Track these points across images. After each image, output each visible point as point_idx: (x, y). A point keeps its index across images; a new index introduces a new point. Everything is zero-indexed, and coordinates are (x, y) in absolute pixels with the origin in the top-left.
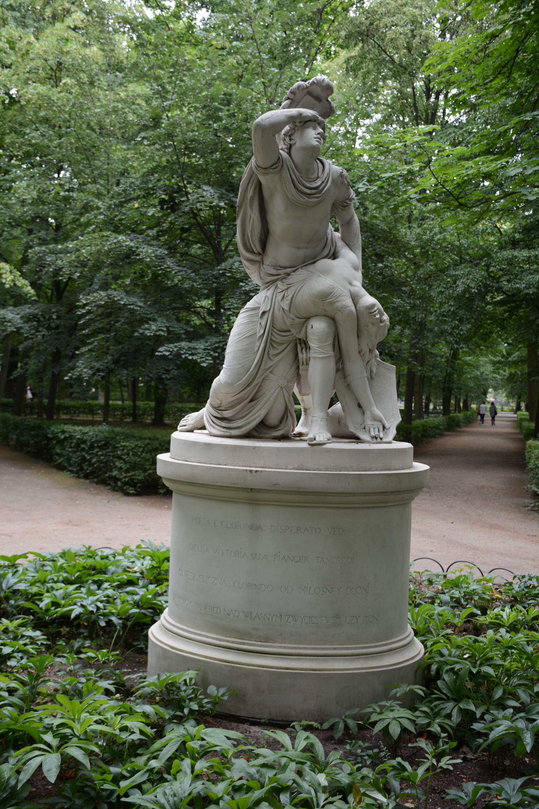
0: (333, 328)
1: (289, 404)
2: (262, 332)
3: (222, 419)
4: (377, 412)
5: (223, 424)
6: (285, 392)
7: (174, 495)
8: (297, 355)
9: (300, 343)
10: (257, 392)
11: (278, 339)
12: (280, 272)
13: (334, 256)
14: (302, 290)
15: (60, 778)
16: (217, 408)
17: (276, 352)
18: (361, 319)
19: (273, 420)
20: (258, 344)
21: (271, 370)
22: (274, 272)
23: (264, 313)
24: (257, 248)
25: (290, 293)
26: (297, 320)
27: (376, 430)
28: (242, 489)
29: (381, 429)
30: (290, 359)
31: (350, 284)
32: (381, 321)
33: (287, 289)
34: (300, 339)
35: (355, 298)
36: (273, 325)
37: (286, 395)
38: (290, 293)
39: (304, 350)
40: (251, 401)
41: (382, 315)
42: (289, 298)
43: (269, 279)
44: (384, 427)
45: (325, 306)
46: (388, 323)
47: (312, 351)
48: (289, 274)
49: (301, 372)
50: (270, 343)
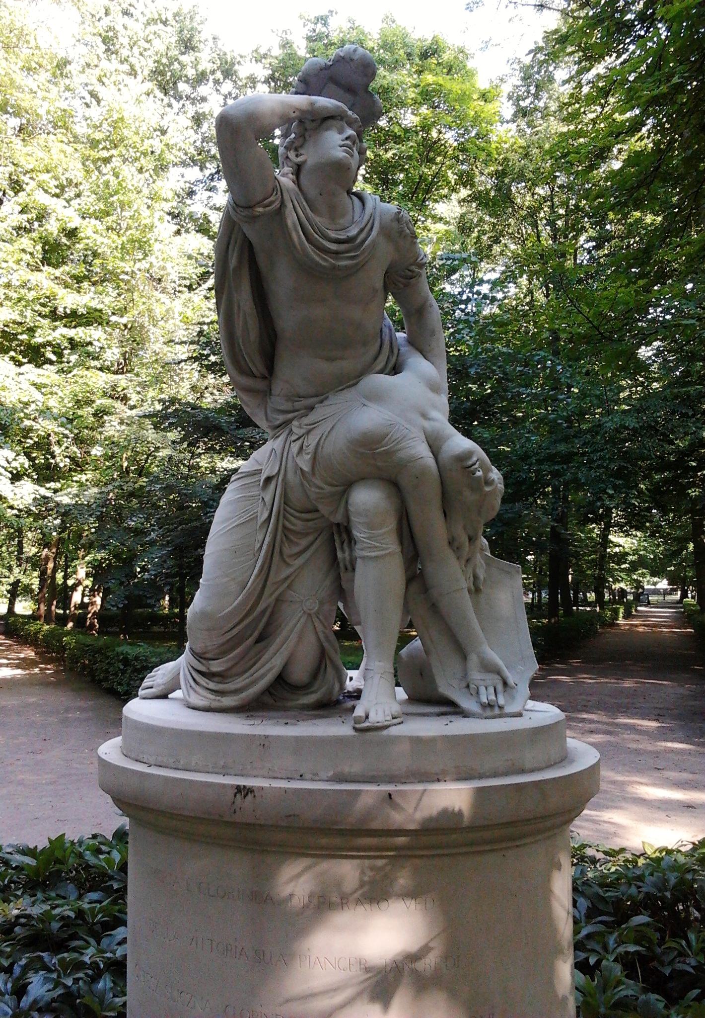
1: (325, 644)
2: (266, 515)
4: (494, 657)
5: (212, 685)
6: (317, 624)
10: (268, 624)
11: (299, 525)
12: (297, 405)
13: (396, 370)
14: (334, 433)
16: (198, 656)
17: (296, 550)
18: (453, 478)
19: (300, 673)
20: (260, 538)
21: (290, 582)
22: (287, 406)
23: (268, 480)
24: (258, 367)
25: (312, 441)
26: (328, 489)
27: (491, 690)
29: (500, 687)
31: (424, 416)
32: (488, 482)
33: (308, 432)
34: (338, 525)
35: (434, 444)
36: (286, 500)
38: (312, 441)
39: (345, 545)
40: (258, 641)
41: (487, 471)
42: (311, 449)
43: (281, 418)
44: (505, 684)
45: (377, 460)
46: (501, 486)
47: (358, 546)
48: (311, 408)
49: (345, 585)
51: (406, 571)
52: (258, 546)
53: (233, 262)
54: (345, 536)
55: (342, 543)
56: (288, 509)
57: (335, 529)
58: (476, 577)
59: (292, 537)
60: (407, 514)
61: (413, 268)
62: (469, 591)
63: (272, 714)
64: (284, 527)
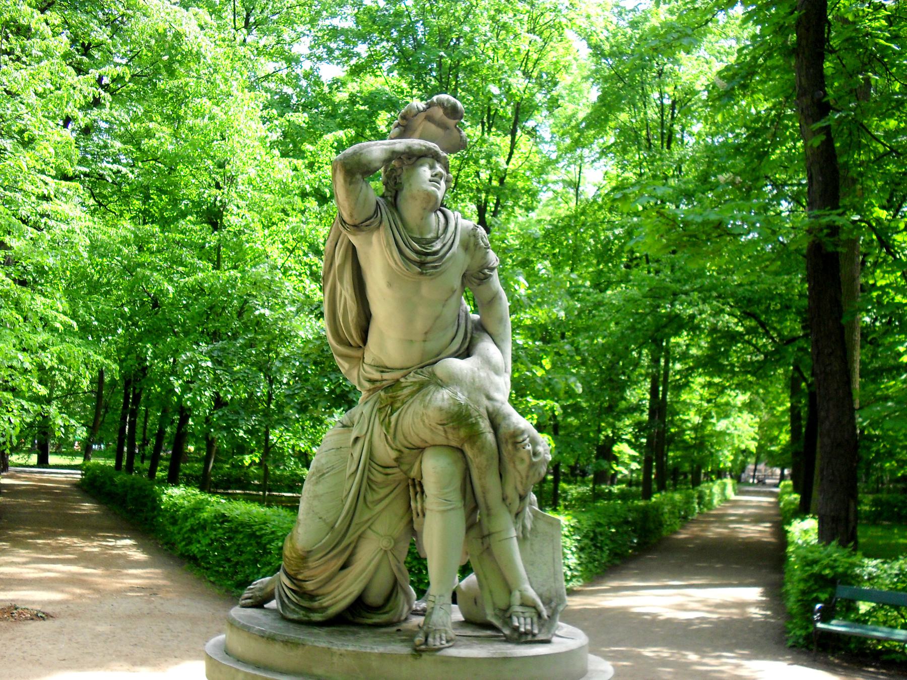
0: (461, 465)
2: (354, 468)
3: (284, 618)
8: (410, 506)
9: (414, 486)
15: (566, 317)
19: (375, 596)
20: (347, 487)
24: (356, 339)
27: (529, 621)
29: (535, 619)
30: (399, 507)
34: (413, 480)
36: (371, 456)
37: (393, 562)
39: (418, 496)
49: (415, 527)
50: (367, 484)
51: (467, 520)
52: (345, 494)
53: (338, 261)
54: (418, 489)
55: (416, 494)
56: (373, 464)
57: (410, 482)
58: (524, 527)
59: (374, 486)
60: (355, 547)
61: (486, 271)
62: (518, 537)
64: (368, 478)
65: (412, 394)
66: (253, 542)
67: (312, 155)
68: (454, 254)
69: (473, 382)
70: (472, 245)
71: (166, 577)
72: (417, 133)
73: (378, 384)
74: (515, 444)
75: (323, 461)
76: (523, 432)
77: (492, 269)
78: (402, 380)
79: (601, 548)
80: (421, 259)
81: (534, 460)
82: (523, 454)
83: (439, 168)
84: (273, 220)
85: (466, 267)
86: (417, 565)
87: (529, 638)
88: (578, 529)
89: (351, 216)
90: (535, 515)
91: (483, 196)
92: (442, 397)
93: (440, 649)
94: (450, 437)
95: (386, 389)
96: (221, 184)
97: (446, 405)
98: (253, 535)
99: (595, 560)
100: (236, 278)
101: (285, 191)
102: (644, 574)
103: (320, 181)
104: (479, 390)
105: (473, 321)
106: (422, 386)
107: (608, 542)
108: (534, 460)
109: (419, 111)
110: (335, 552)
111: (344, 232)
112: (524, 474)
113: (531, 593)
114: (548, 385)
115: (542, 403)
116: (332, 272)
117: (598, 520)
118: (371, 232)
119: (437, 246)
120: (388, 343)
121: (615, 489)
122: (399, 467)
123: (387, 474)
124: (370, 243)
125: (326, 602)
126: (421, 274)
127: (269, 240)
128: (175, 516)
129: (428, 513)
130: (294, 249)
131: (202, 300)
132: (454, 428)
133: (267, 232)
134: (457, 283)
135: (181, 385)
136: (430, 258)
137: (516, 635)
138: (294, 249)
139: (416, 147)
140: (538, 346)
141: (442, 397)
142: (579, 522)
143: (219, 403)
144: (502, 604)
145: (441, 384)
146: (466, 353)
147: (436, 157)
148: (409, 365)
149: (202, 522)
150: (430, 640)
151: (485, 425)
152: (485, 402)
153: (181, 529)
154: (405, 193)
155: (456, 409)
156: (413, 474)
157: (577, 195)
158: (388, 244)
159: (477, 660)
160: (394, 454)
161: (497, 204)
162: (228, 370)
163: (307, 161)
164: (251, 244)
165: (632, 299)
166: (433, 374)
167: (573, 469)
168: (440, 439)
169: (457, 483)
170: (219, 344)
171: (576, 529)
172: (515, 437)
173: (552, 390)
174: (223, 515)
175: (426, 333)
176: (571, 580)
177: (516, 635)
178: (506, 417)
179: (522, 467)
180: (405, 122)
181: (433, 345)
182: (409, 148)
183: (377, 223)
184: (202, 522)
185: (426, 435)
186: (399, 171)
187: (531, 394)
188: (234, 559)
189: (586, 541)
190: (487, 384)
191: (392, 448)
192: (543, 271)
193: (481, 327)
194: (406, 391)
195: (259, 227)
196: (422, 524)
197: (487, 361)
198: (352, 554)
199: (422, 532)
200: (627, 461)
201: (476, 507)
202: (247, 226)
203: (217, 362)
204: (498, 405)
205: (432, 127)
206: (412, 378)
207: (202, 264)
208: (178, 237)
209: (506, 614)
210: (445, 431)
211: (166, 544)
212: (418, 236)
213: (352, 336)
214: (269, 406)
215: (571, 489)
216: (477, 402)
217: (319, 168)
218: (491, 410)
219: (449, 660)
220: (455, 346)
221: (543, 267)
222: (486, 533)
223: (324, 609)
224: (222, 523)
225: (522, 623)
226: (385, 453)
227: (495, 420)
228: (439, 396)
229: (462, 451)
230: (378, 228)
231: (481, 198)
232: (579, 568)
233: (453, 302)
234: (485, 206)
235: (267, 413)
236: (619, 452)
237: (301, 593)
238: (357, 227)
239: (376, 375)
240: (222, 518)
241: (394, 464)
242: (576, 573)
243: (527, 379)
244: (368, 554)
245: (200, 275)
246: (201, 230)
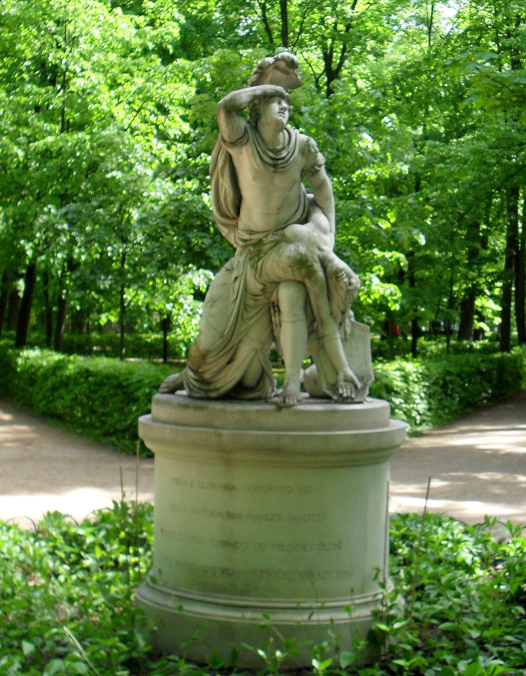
2: (235, 296)
7: (157, 458)
8: (271, 321)
9: (274, 307)
19: (251, 380)
24: (232, 212)
27: (349, 390)
28: (347, 453)
29: (353, 389)
30: (264, 321)
34: (273, 303)
37: (261, 357)
50: (244, 307)
53: (220, 164)
54: (276, 309)
55: (275, 312)
57: (271, 305)
58: (345, 332)
60: (237, 348)
61: (316, 167)
62: (342, 339)
63: (485, 414)
65: (271, 248)
66: (120, 392)
67: (153, 12)
68: (295, 159)
69: (310, 239)
70: (306, 152)
71: (35, 431)
72: (269, 78)
73: (248, 243)
74: (337, 278)
75: (215, 293)
76: (341, 270)
77: (320, 166)
78: (264, 239)
79: (451, 396)
80: (274, 163)
81: (350, 288)
82: (342, 284)
83: (284, 104)
84: (119, 81)
85: (302, 166)
86: (276, 357)
87: (350, 400)
88: (427, 376)
89: (230, 137)
90: (353, 324)
91: (329, 42)
92: (290, 250)
93: (293, 406)
94: (296, 274)
95: (254, 245)
96: (63, 44)
97: (293, 254)
98: (120, 386)
99: (444, 407)
100: (85, 141)
101: (127, 50)
102: (495, 420)
103: (162, 37)
104: (312, 244)
105: (309, 200)
106: (277, 243)
107: (459, 390)
108: (350, 288)
109: (270, 65)
110: (220, 354)
111: (224, 146)
112: (343, 297)
113: (351, 373)
114: (392, 237)
115: (388, 255)
116: (216, 171)
117: (448, 369)
118: (242, 146)
119: (284, 154)
120: (255, 214)
121: (477, 345)
122: (263, 294)
123: (256, 300)
124: (241, 153)
125: (218, 385)
126: (274, 172)
127: (115, 101)
128: (33, 376)
129: (283, 324)
130: (140, 110)
131: (51, 163)
132: (298, 269)
133: (112, 93)
134: (297, 176)
135: (31, 248)
136: (280, 162)
137: (341, 399)
138: (140, 110)
139: (269, 91)
140: (382, 201)
141: (290, 250)
142: (428, 369)
143: (72, 264)
144: (332, 380)
145: (289, 241)
146: (305, 220)
147: (281, 96)
148: (267, 229)
149: (64, 379)
150: (287, 400)
151: (317, 266)
152: (318, 252)
153: (41, 388)
154: (263, 120)
155: (299, 257)
156: (273, 299)
157: (429, 33)
158: (253, 154)
159: (316, 412)
160: (260, 287)
161: (344, 50)
162: (82, 230)
163: (148, 19)
164: (97, 105)
165: (479, 151)
166: (284, 235)
167: (435, 324)
168: (289, 276)
169: (301, 303)
170: (72, 206)
171: (425, 377)
172: (337, 273)
173: (396, 241)
174: (87, 371)
175: (278, 209)
176: (420, 424)
177: (341, 399)
178: (331, 261)
179: (342, 293)
180: (260, 71)
181: (284, 216)
182: (265, 92)
183: (245, 141)
184: (64, 379)
185: (281, 274)
186: (258, 106)
187: (377, 247)
188: (101, 410)
189: (436, 388)
190: (318, 240)
191: (259, 283)
192: (390, 124)
193: (314, 203)
194: (267, 247)
195: (104, 88)
196: (279, 332)
197: (319, 226)
198: (235, 354)
199: (279, 337)
200: (490, 316)
201: (314, 320)
202: (93, 87)
203: (71, 223)
204: (326, 253)
205: (279, 74)
206: (271, 238)
207: (47, 126)
208: (23, 99)
209: (334, 387)
210: (293, 271)
211: (25, 405)
212: (271, 147)
213: (229, 211)
214: (123, 265)
215: (431, 345)
216: (313, 252)
217: (161, 24)
218: (321, 256)
219: (298, 413)
220: (298, 216)
221: (390, 121)
222: (320, 335)
223: (218, 389)
224: (87, 378)
225: (345, 391)
226: (255, 286)
227: (324, 262)
228: (288, 249)
229: (302, 283)
230: (246, 143)
231: (326, 44)
232: (428, 413)
233: (295, 188)
234: (332, 52)
235: (121, 273)
236: (482, 307)
237: (202, 381)
238: (233, 144)
239: (247, 237)
240: (87, 373)
241: (259, 293)
242: (425, 418)
243: (372, 232)
244: (245, 353)
245: (50, 139)
246: (46, 93)
